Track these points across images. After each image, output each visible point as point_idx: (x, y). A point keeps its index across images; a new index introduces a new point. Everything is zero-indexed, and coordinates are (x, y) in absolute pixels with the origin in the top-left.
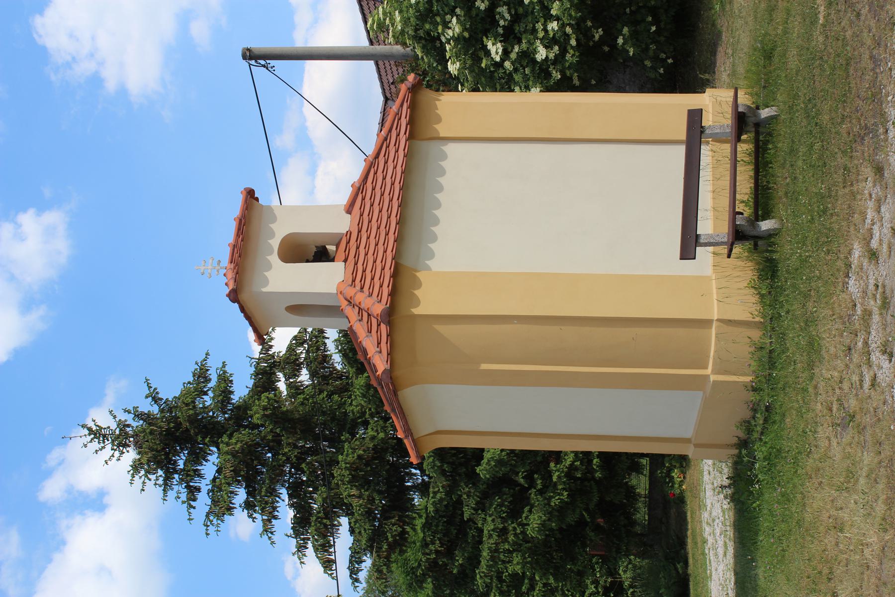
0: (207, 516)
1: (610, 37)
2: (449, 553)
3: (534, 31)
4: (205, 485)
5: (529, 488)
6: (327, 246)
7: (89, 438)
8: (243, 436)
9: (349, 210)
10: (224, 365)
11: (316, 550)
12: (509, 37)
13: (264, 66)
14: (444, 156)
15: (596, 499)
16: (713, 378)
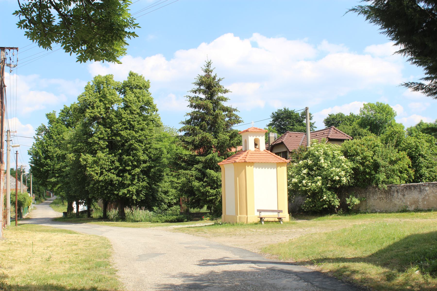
0: (189, 96)
1: (309, 197)
2: (184, 161)
3: (309, 180)
4: (197, 95)
5: (203, 182)
7: (207, 62)
8: (211, 106)
10: (229, 99)
11: (183, 127)
12: (308, 174)
14: (274, 169)
15: (202, 198)
16: (238, 216)
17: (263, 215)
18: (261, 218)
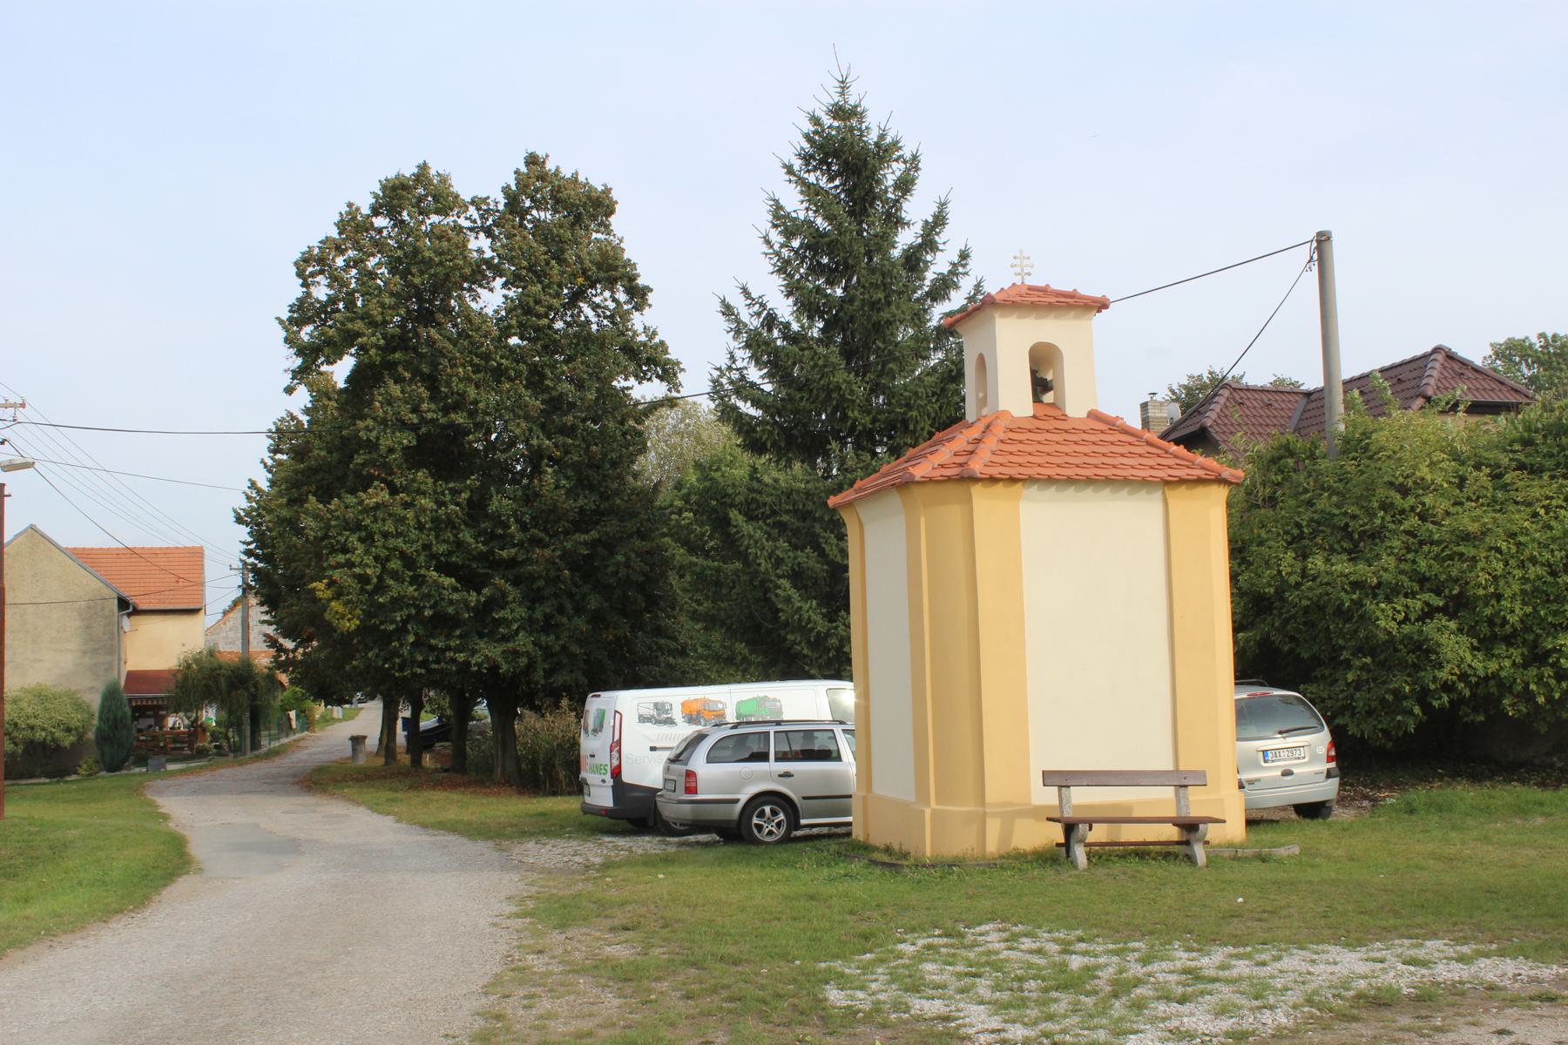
6: (1052, 392)
7: (882, 128)
9: (1094, 415)
10: (844, 86)
13: (1311, 258)
16: (928, 812)
17: (1083, 797)
18: (1070, 828)
